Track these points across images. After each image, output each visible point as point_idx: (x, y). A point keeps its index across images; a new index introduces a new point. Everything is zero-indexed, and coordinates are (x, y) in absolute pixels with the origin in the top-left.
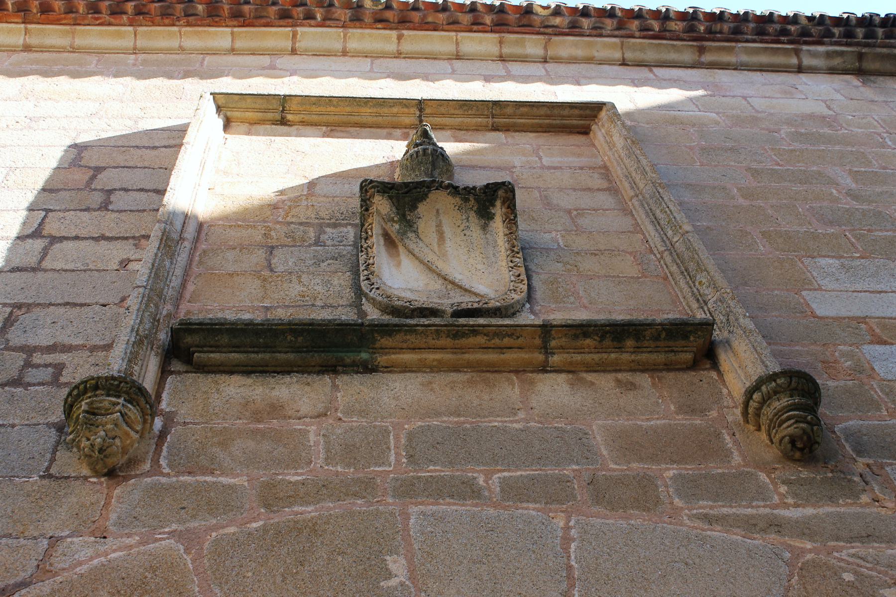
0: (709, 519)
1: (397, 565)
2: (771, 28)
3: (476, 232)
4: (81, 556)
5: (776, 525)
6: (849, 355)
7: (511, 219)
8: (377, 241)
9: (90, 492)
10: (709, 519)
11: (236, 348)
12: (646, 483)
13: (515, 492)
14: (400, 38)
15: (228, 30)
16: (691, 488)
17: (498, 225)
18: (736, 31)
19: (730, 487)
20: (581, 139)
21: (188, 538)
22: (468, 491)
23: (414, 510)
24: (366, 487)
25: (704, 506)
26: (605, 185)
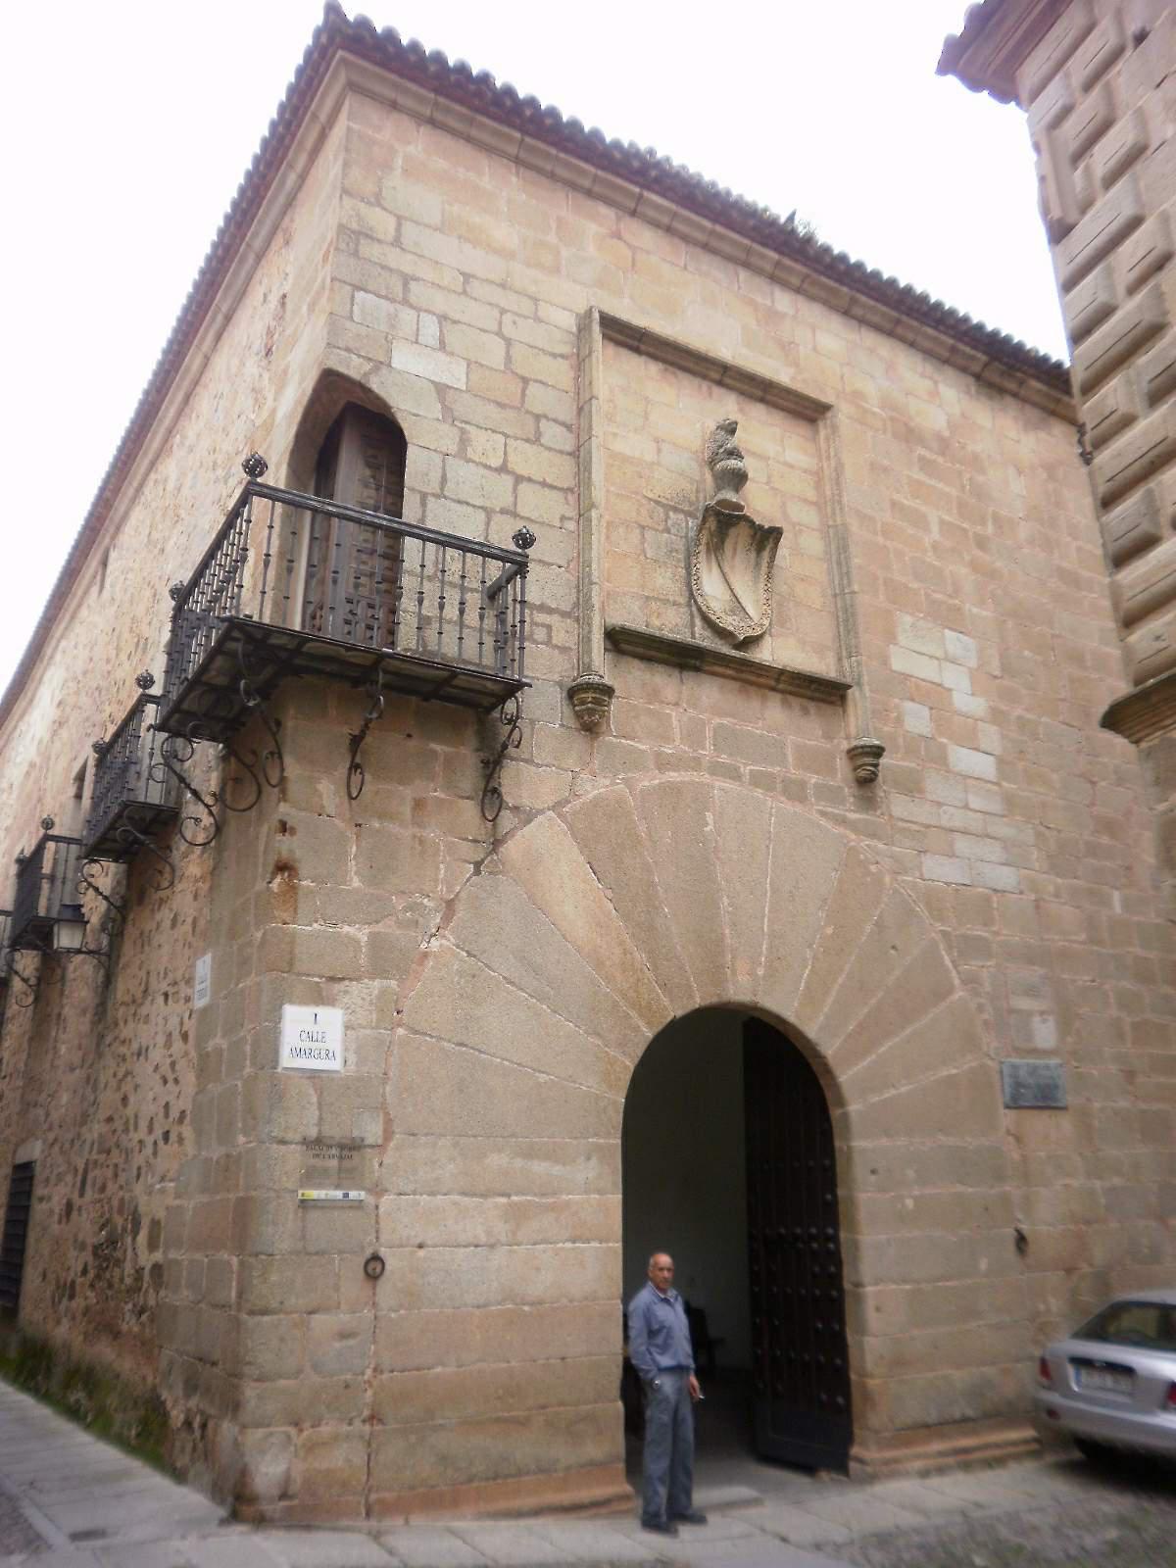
0: (823, 814)
3: (753, 555)
8: (702, 548)
9: (580, 741)
12: (803, 784)
13: (757, 780)
16: (822, 792)
17: (766, 554)
20: (802, 429)
22: (734, 774)
23: (717, 784)
24: (696, 764)
26: (811, 495)
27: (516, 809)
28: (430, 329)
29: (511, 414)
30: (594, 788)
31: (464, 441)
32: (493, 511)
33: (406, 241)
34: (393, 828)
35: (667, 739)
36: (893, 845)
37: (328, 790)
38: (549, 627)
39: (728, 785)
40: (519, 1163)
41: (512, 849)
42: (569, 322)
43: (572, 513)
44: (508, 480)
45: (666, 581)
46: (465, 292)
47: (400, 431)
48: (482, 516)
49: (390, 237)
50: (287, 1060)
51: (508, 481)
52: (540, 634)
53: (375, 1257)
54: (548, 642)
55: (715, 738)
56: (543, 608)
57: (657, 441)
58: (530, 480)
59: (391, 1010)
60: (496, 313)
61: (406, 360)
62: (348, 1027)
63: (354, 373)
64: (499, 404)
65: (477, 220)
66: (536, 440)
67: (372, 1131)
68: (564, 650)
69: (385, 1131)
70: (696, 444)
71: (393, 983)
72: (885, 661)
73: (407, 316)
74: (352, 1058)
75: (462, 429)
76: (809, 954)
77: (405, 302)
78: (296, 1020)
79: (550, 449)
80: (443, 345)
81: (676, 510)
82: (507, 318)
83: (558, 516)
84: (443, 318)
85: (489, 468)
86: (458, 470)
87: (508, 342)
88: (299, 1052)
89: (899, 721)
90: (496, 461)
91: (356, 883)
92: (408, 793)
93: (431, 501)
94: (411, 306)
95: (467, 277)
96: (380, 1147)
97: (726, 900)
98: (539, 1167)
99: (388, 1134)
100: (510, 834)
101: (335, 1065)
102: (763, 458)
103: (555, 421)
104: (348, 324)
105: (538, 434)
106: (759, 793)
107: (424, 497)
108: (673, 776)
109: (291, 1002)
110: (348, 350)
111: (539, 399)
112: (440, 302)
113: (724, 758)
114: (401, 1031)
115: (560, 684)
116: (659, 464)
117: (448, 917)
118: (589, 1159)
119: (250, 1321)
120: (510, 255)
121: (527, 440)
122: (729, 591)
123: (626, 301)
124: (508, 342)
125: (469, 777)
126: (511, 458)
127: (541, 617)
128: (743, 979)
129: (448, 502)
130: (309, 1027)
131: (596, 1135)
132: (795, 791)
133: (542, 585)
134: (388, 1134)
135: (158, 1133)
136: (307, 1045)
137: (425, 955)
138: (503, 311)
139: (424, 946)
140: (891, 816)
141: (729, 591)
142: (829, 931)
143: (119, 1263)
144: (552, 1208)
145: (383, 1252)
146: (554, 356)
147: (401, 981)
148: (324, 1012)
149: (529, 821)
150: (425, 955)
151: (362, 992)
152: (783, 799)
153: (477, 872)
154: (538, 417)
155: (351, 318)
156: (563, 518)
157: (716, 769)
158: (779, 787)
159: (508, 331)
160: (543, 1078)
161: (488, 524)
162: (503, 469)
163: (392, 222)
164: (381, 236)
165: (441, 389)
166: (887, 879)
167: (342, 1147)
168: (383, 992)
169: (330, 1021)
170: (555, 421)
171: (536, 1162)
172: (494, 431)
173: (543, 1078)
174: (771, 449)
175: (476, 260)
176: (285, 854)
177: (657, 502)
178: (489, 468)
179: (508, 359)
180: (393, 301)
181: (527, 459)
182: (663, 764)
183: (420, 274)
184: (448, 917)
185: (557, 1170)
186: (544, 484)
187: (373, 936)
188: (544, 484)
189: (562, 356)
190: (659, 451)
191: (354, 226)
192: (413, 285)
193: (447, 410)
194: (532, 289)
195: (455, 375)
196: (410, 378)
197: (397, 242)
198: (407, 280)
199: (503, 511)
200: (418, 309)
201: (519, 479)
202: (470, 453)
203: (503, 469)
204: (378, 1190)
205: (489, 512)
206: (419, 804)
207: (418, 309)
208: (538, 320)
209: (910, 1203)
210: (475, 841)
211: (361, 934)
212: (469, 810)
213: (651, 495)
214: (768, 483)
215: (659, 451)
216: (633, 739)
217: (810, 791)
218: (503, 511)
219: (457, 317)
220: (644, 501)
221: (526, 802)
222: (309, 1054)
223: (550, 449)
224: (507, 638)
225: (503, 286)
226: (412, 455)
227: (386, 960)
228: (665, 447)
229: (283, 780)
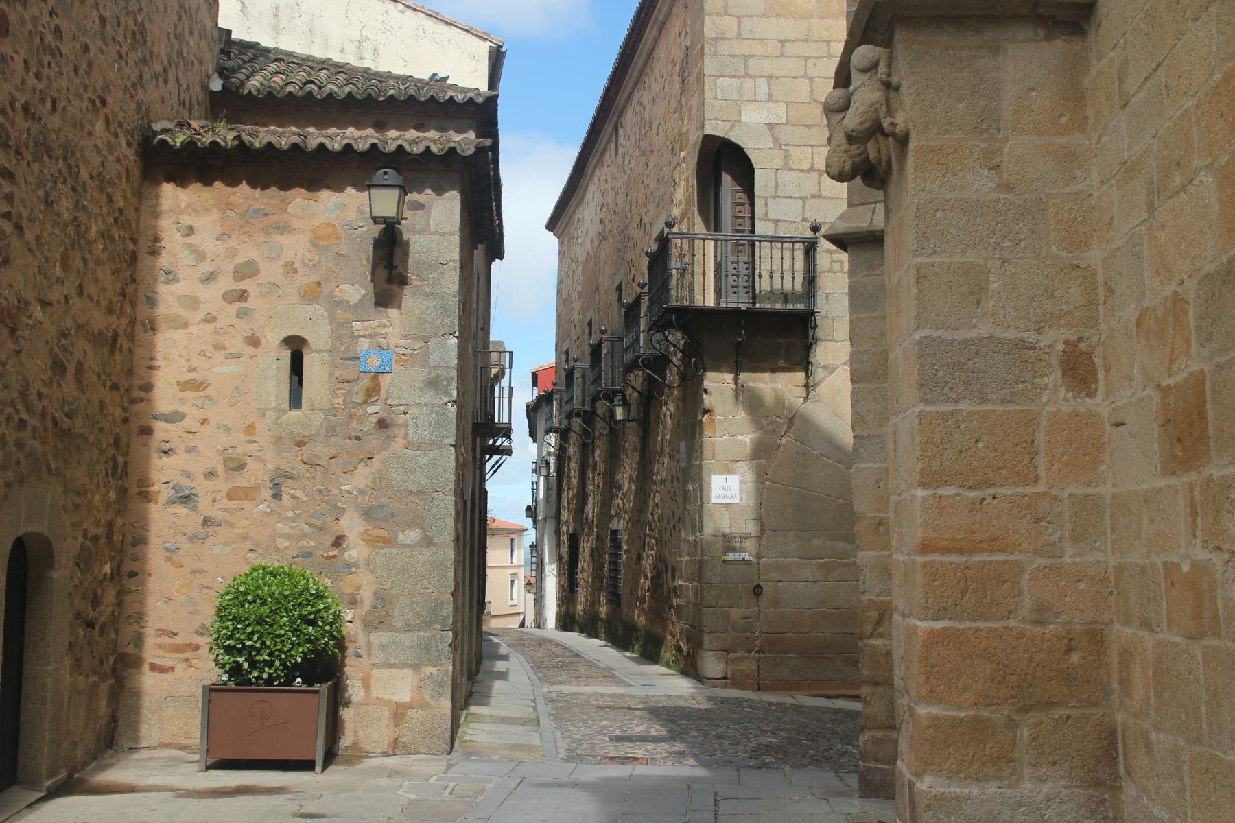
27: (825, 367)
28: (762, 85)
31: (787, 157)
33: (745, 33)
40: (829, 543)
41: (823, 389)
46: (782, 55)
47: (742, 149)
48: (800, 202)
49: (735, 34)
50: (714, 500)
53: (758, 586)
60: (802, 62)
61: (753, 115)
63: (720, 134)
64: (808, 126)
73: (748, 83)
74: (744, 497)
77: (747, 75)
80: (771, 97)
85: (802, 171)
86: (786, 178)
87: (811, 79)
88: (719, 496)
90: (806, 166)
93: (770, 202)
94: (750, 77)
100: (815, 386)
101: (737, 500)
104: (715, 102)
107: (766, 199)
110: (716, 119)
112: (769, 67)
117: (789, 427)
119: (705, 610)
120: (806, 15)
124: (811, 79)
130: (724, 484)
135: (671, 526)
137: (779, 446)
143: (662, 586)
144: (847, 565)
147: (767, 459)
148: (730, 477)
150: (779, 446)
155: (716, 98)
159: (812, 72)
160: (841, 501)
163: (734, 21)
164: (729, 36)
165: (771, 126)
171: (274, 383)
173: (841, 501)
175: (789, 28)
178: (802, 171)
179: (812, 92)
184: (789, 427)
191: (714, 36)
193: (776, 140)
195: (777, 114)
199: (813, 197)
200: (754, 77)
202: (791, 165)
205: (803, 199)
207: (754, 77)
218: (813, 197)
219: (778, 74)
221: (831, 362)
225: (806, 40)
226: (758, 174)
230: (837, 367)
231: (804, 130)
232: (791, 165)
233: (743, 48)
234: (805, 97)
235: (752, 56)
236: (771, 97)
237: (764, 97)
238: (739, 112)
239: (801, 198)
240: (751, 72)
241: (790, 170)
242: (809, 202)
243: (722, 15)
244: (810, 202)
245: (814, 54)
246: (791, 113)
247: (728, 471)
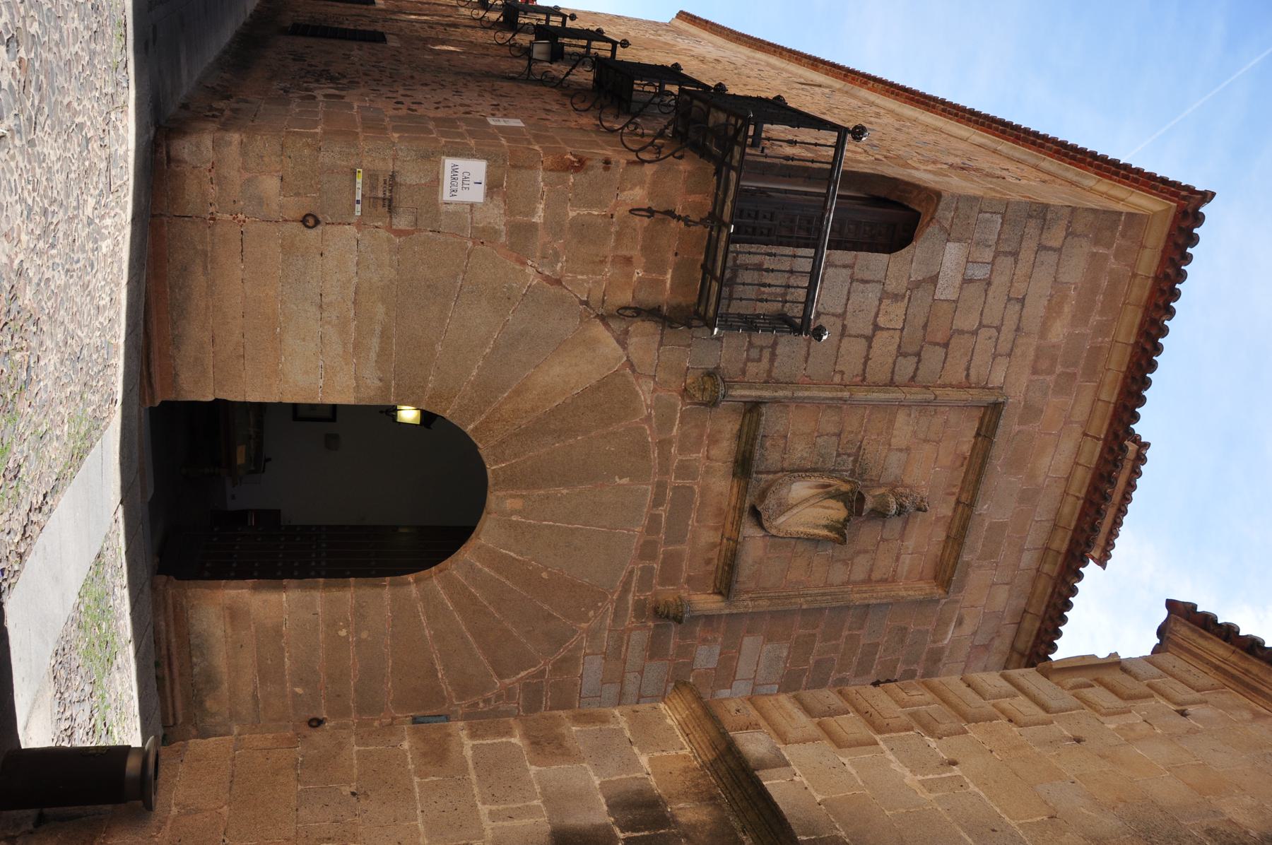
1: (625, 481)
2: (1126, 417)
4: (644, 388)
5: (626, 590)
6: (715, 640)
7: (834, 541)
10: (631, 572)
11: (990, 421)
12: (653, 557)
13: (654, 519)
14: (1078, 498)
15: (1113, 400)
16: (647, 571)
18: (1140, 366)
19: (645, 583)
21: (649, 417)
22: (657, 502)
24: (664, 470)
25: (637, 574)
26: (876, 575)
29: (920, 333)
30: (645, 392)
31: (896, 297)
32: (844, 319)
34: (612, 242)
35: (682, 450)
36: (610, 631)
37: (637, 195)
38: (759, 360)
39: (649, 497)
40: (378, 328)
41: (599, 330)
42: (997, 378)
43: (847, 380)
44: (868, 331)
45: (800, 452)
46: (1009, 299)
49: (1045, 243)
50: (449, 162)
51: (868, 331)
52: (754, 353)
53: (317, 222)
54: (748, 359)
55: (684, 487)
56: (773, 356)
57: (908, 449)
58: (870, 347)
59: (484, 235)
61: (953, 253)
62: (472, 205)
64: (925, 326)
65: (1066, 309)
66: (901, 353)
67: (402, 222)
68: (744, 372)
69: (401, 231)
70: (908, 481)
71: (503, 239)
72: (750, 632)
73: (988, 255)
75: (904, 295)
76: (526, 558)
78: (477, 169)
79: (894, 363)
81: (855, 461)
82: (994, 332)
83: (843, 369)
84: (989, 283)
85: (877, 315)
89: (705, 641)
90: (881, 321)
91: (572, 214)
92: (636, 253)
93: (847, 272)
94: (995, 257)
95: (1022, 301)
96: (390, 228)
97: (565, 492)
98: (375, 343)
99: (399, 233)
100: (607, 325)
101: (446, 196)
102: (902, 536)
103: (917, 369)
105: (905, 355)
106: (645, 521)
108: (655, 454)
109: (488, 167)
110: (957, 209)
111: (933, 357)
112: (1000, 280)
113: (669, 494)
114: (470, 244)
115: (717, 368)
116: (890, 450)
118: (380, 380)
121: (899, 346)
122: (805, 508)
123: (1017, 428)
125: (648, 298)
126: (885, 334)
127: (766, 353)
128: (509, 504)
129: (847, 284)
130: (473, 179)
131: (398, 385)
132: (647, 551)
133: (790, 347)
134: (399, 233)
136: (460, 177)
138: (999, 330)
139: (530, 262)
140: (631, 630)
141: (805, 508)
142: (544, 575)
145: (320, 227)
146: (968, 369)
147: (503, 246)
149: (618, 341)
150: (524, 263)
151: (496, 217)
152: (641, 541)
153: (582, 302)
154: (918, 355)
155: (981, 211)
156: (842, 373)
157: (661, 487)
158: (649, 538)
159: (984, 333)
161: (833, 315)
162: (876, 327)
165: (934, 280)
166: (584, 625)
167: (390, 200)
168: (497, 232)
169: (477, 194)
170: (917, 369)
172: (905, 320)
174: (910, 543)
176: (588, 163)
177: (860, 447)
178: (877, 315)
179: (961, 332)
180: (997, 243)
181: (885, 346)
182: (664, 444)
183: (1019, 265)
185: (373, 356)
186: (867, 359)
187: (534, 225)
188: (867, 359)
189: (968, 376)
190: (901, 450)
192: (1011, 260)
193: (918, 285)
194: (1018, 351)
195: (946, 290)
196: (944, 258)
197: (1042, 248)
198: (1015, 254)
199: (844, 327)
200: (993, 263)
201: (869, 339)
203: (876, 327)
204: (360, 225)
205: (843, 316)
206: (628, 260)
207: (993, 263)
208: (995, 357)
209: (343, 633)
210: (603, 301)
211: (538, 218)
212: (625, 297)
213: (865, 442)
214: (883, 540)
215: (901, 450)
216: (681, 422)
217: (647, 563)
218: (844, 327)
220: (860, 437)
222: (454, 179)
223: (894, 363)
224: (750, 324)
225: (1018, 329)
226: (878, 260)
227: (522, 233)
228: (903, 456)
229: (643, 162)
230: (625, 348)
231: (922, 322)
232: (886, 302)
233: (1026, 255)
234: (959, 324)
235: (1016, 263)
236: (967, 281)
237: (970, 273)
238: (959, 240)
239: (845, 312)
240: (999, 260)
241: (880, 301)
242: (839, 322)
243: (1068, 227)
244: (839, 322)
245: (1001, 339)
246: (945, 304)
247: (493, 187)
